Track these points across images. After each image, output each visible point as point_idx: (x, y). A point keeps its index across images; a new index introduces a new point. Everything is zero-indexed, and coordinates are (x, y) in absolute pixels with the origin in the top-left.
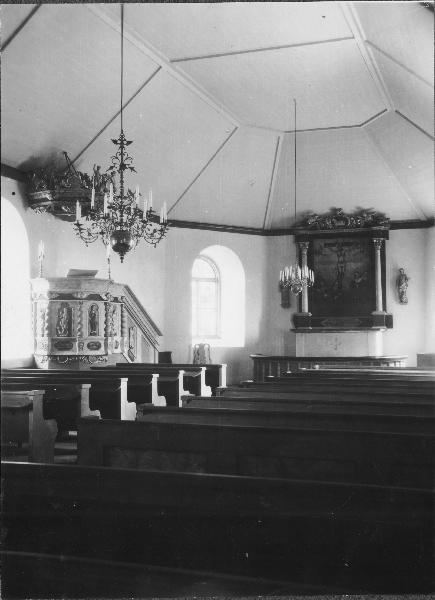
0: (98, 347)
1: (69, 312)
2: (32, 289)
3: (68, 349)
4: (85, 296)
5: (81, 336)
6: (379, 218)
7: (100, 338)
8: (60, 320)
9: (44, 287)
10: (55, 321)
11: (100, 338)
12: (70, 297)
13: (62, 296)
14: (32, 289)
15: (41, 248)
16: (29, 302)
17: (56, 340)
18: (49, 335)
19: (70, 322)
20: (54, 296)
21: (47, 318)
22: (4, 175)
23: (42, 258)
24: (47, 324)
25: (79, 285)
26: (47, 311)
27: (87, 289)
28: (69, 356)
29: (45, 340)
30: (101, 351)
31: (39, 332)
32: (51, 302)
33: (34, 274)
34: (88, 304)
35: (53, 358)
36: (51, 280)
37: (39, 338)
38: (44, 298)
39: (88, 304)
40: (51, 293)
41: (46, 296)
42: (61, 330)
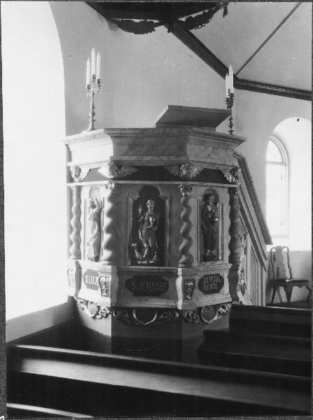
0: (217, 289)
1: (160, 207)
2: (70, 159)
3: (158, 294)
4: (195, 171)
5: (187, 264)
6: (280, 247)
7: (222, 267)
8: (137, 226)
9: (98, 152)
10: (126, 231)
11: (222, 267)
12: (161, 173)
13: (143, 172)
14: (70, 159)
15: (93, 66)
16: (63, 185)
17: (129, 272)
18: (111, 260)
19: (160, 231)
20: (125, 171)
21: (106, 221)
22: (105, 337)
23: (94, 89)
24: (106, 237)
25: (181, 149)
26: (108, 206)
27: (198, 154)
28: (160, 311)
29: (103, 270)
30: (223, 296)
31: (88, 250)
32: (118, 187)
33: (74, 126)
34: (199, 191)
35: (119, 312)
36: (118, 136)
37: (87, 264)
38: (104, 178)
39: (199, 191)
40: (116, 165)
41: (105, 171)
42: (140, 249)
